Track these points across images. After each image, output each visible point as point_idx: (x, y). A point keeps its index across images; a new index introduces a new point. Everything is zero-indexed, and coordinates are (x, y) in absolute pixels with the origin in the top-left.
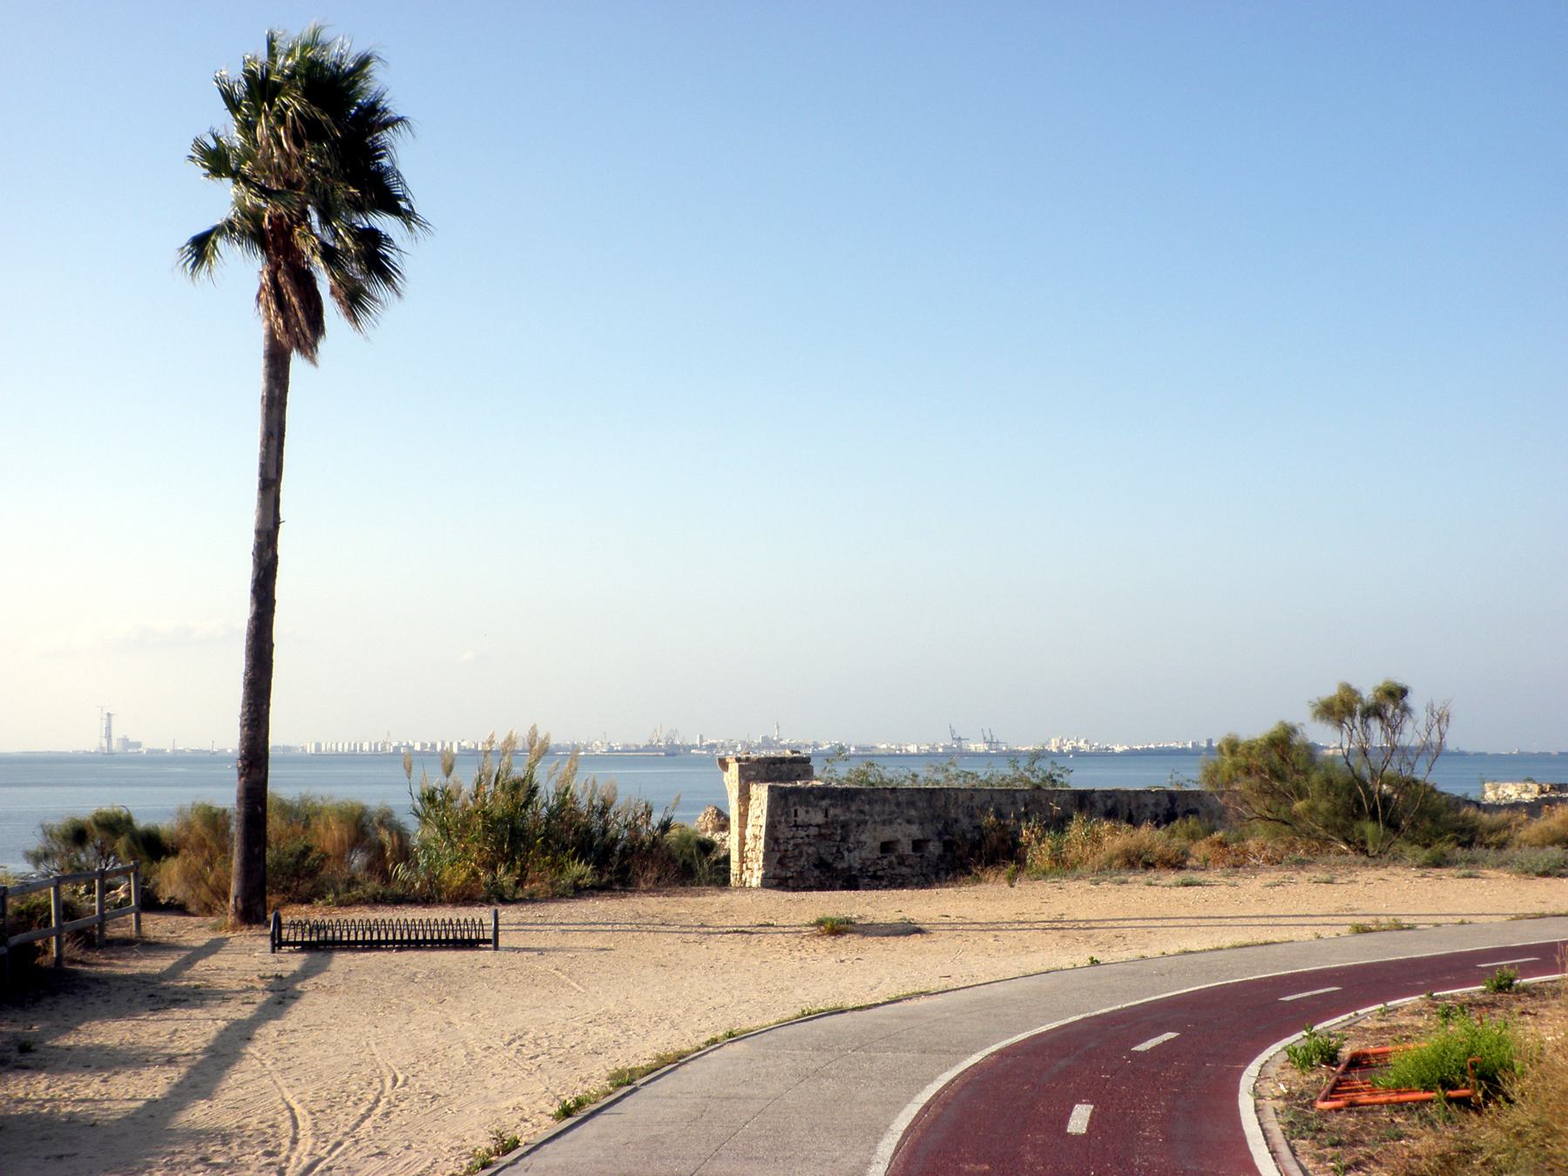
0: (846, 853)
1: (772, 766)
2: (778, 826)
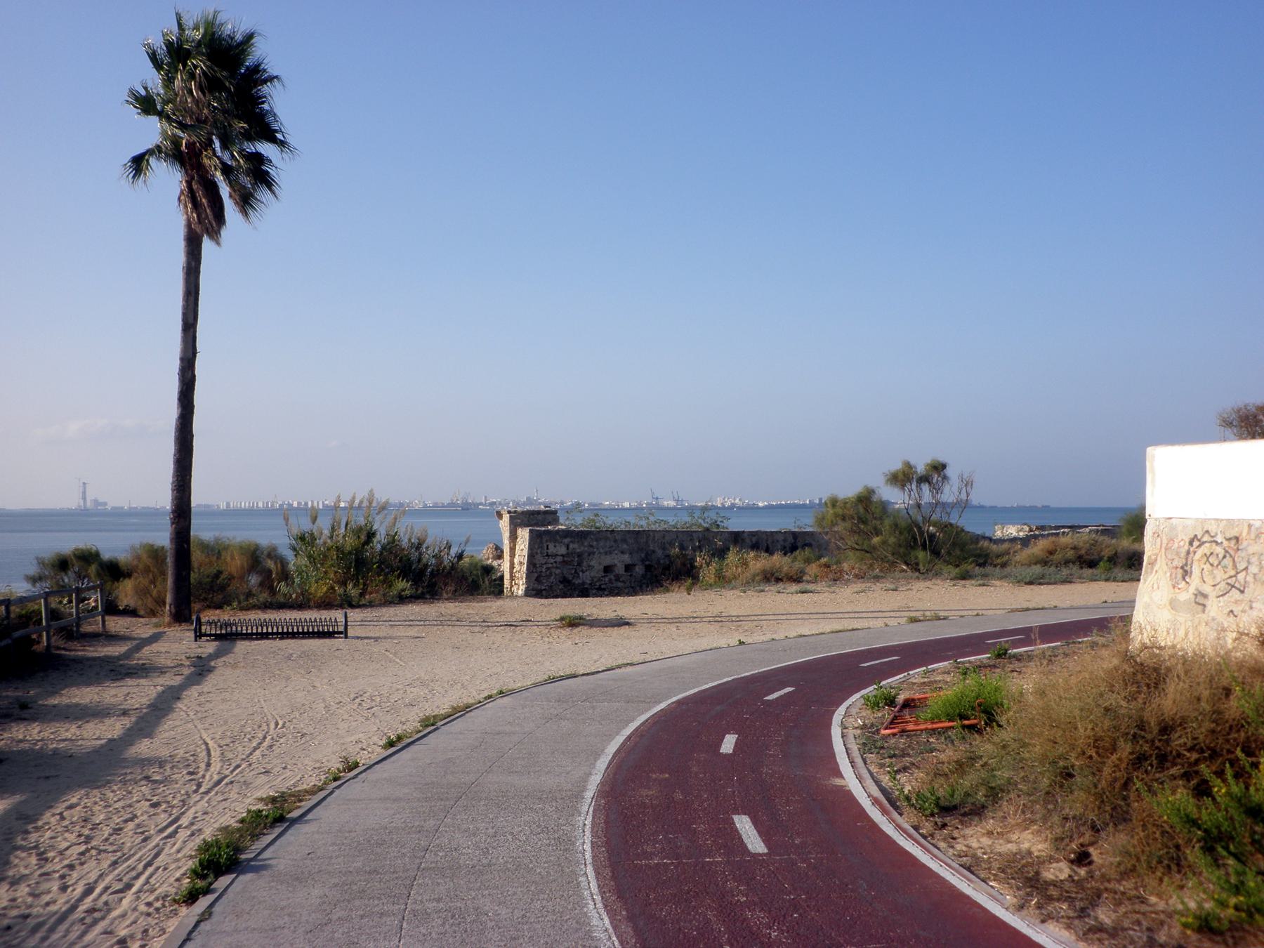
0: (581, 574)
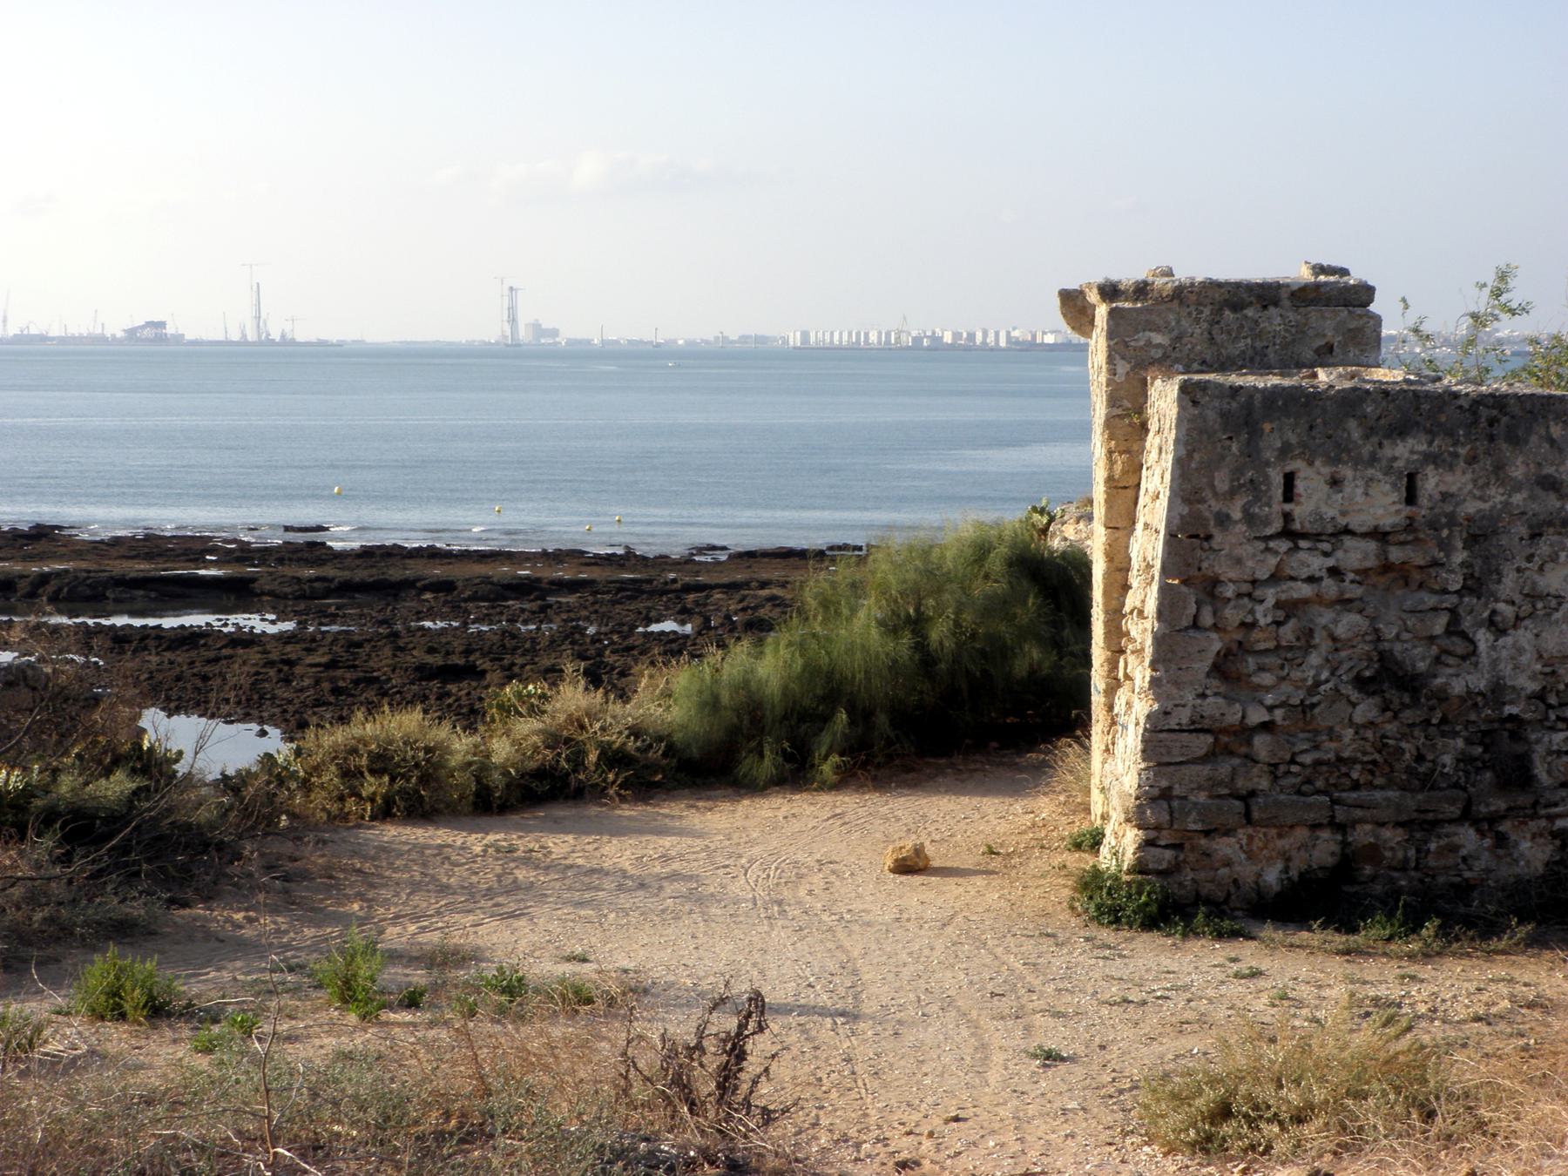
0: (1483, 638)
1: (1228, 314)
2: (1218, 538)
